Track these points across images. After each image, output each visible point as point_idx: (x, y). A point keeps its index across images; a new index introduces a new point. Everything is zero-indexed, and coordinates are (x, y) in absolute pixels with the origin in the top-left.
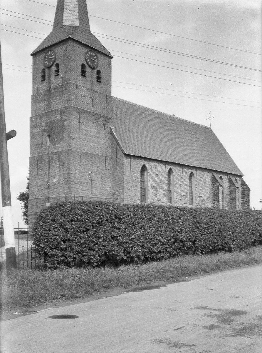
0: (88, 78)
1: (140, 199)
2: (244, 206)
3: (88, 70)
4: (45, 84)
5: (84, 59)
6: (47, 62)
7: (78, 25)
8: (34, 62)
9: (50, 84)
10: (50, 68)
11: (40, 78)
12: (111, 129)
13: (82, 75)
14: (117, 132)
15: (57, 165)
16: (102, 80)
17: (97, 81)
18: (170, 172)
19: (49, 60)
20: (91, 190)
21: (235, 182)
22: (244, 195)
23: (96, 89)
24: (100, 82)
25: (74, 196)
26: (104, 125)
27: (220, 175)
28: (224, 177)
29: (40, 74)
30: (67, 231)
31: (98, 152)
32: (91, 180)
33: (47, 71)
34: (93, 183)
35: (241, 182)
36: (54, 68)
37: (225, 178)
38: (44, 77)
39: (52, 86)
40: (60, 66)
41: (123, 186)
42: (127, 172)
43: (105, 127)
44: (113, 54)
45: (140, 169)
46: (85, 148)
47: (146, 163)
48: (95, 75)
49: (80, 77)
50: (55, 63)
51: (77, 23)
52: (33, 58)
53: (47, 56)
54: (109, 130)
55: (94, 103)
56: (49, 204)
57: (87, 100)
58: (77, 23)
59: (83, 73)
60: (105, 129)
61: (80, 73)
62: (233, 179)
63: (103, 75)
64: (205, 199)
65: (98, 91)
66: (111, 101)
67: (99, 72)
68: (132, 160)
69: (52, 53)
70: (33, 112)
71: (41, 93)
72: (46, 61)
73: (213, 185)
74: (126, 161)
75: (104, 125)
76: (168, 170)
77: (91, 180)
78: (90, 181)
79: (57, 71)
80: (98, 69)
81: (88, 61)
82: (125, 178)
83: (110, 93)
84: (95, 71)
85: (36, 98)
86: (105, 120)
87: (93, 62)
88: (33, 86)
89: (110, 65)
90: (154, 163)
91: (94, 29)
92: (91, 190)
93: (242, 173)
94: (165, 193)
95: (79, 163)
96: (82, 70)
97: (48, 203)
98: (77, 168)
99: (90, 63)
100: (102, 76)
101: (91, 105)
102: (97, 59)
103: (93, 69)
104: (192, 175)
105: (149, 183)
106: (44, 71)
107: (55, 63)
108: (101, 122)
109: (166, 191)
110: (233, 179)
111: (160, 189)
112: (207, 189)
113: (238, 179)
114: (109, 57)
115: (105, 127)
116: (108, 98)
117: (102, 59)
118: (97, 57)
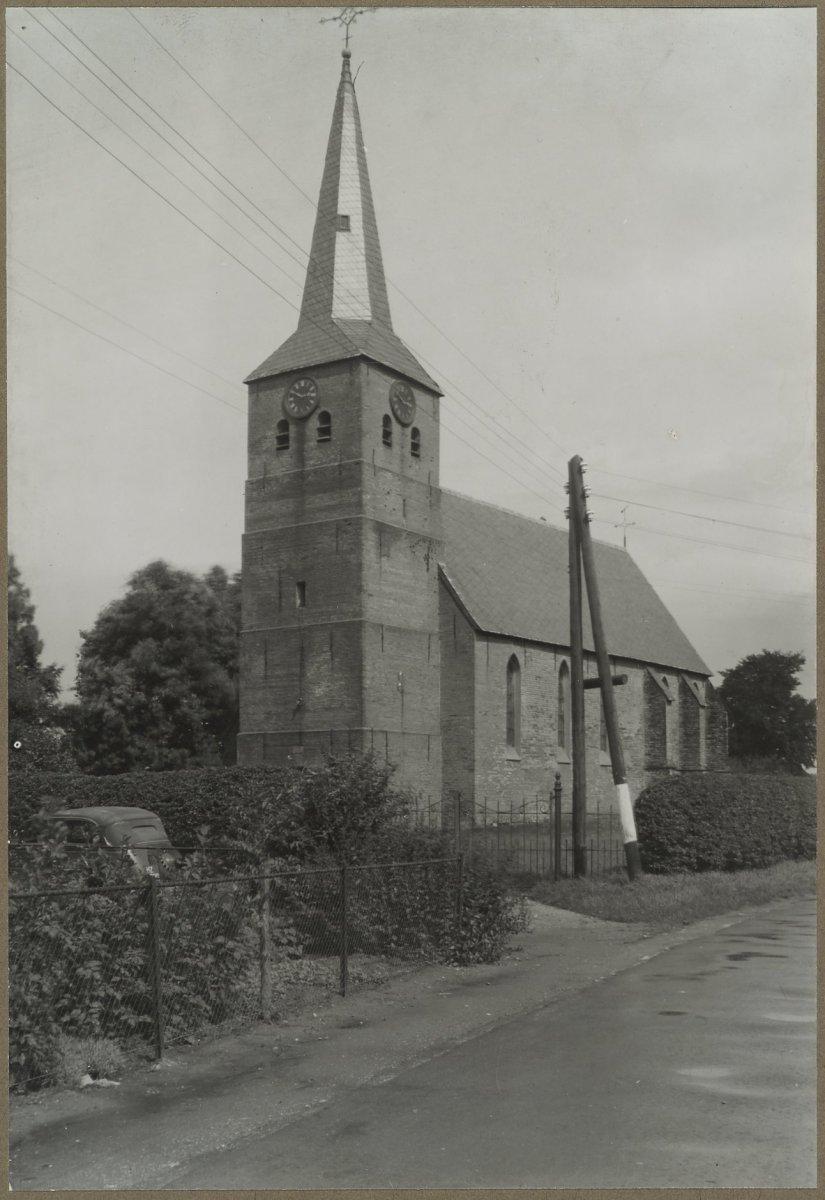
0: (396, 448)
1: (505, 736)
2: (713, 751)
3: (396, 428)
4: (287, 458)
5: (389, 405)
6: (293, 405)
7: (370, 319)
8: (254, 403)
9: (301, 458)
10: (303, 420)
11: (271, 442)
12: (440, 569)
13: (385, 443)
14: (454, 576)
15: (327, 656)
16: (422, 452)
17: (413, 455)
18: (513, 665)
19: (300, 402)
20: (402, 716)
21: (662, 685)
22: (714, 725)
23: (410, 473)
24: (417, 456)
25: (372, 731)
26: (427, 558)
27: (663, 675)
28: (669, 678)
29: (272, 433)
30: (692, 819)
31: (416, 623)
32: (402, 692)
33: (293, 430)
34: (407, 698)
35: (707, 690)
36: (314, 424)
37: (673, 680)
38: (283, 441)
39: (310, 465)
40: (333, 420)
41: (472, 708)
42: (480, 673)
43: (427, 564)
44: (443, 387)
45: (506, 665)
46: (390, 616)
47: (517, 650)
48: (409, 440)
49: (381, 448)
50: (319, 411)
51: (366, 314)
52: (251, 393)
53: (295, 389)
54: (436, 570)
55: (407, 508)
56: (302, 748)
57: (394, 501)
58: (366, 314)
59: (387, 435)
60: (428, 569)
61: (380, 439)
62: (691, 682)
63: (423, 441)
64: (632, 735)
65: (414, 478)
66: (438, 500)
67: (416, 433)
68: (490, 644)
69: (311, 385)
70: (249, 523)
71: (276, 479)
72: (291, 402)
73: (650, 701)
74: (480, 646)
75: (427, 558)
76: (558, 665)
77: (402, 692)
78: (399, 695)
79: (325, 431)
80: (414, 425)
81: (396, 407)
82: (478, 687)
83: (437, 480)
84: (409, 431)
85: (258, 490)
86: (429, 548)
87: (405, 409)
88: (251, 460)
89: (435, 414)
90: (533, 650)
91: (399, 329)
92: (402, 716)
93: (708, 669)
94: (552, 721)
95: (381, 653)
96: (384, 431)
97: (300, 744)
98: (377, 665)
99: (399, 413)
100: (421, 443)
101: (401, 514)
102: (413, 401)
103: (404, 425)
104: (513, 665)
105: (524, 698)
106: (283, 426)
107: (319, 411)
108: (421, 552)
109: (556, 717)
110: (691, 682)
111: (543, 713)
112: (635, 708)
113: (700, 684)
114: (436, 395)
115: (427, 564)
116: (435, 494)
117: (422, 398)
118: (412, 396)
